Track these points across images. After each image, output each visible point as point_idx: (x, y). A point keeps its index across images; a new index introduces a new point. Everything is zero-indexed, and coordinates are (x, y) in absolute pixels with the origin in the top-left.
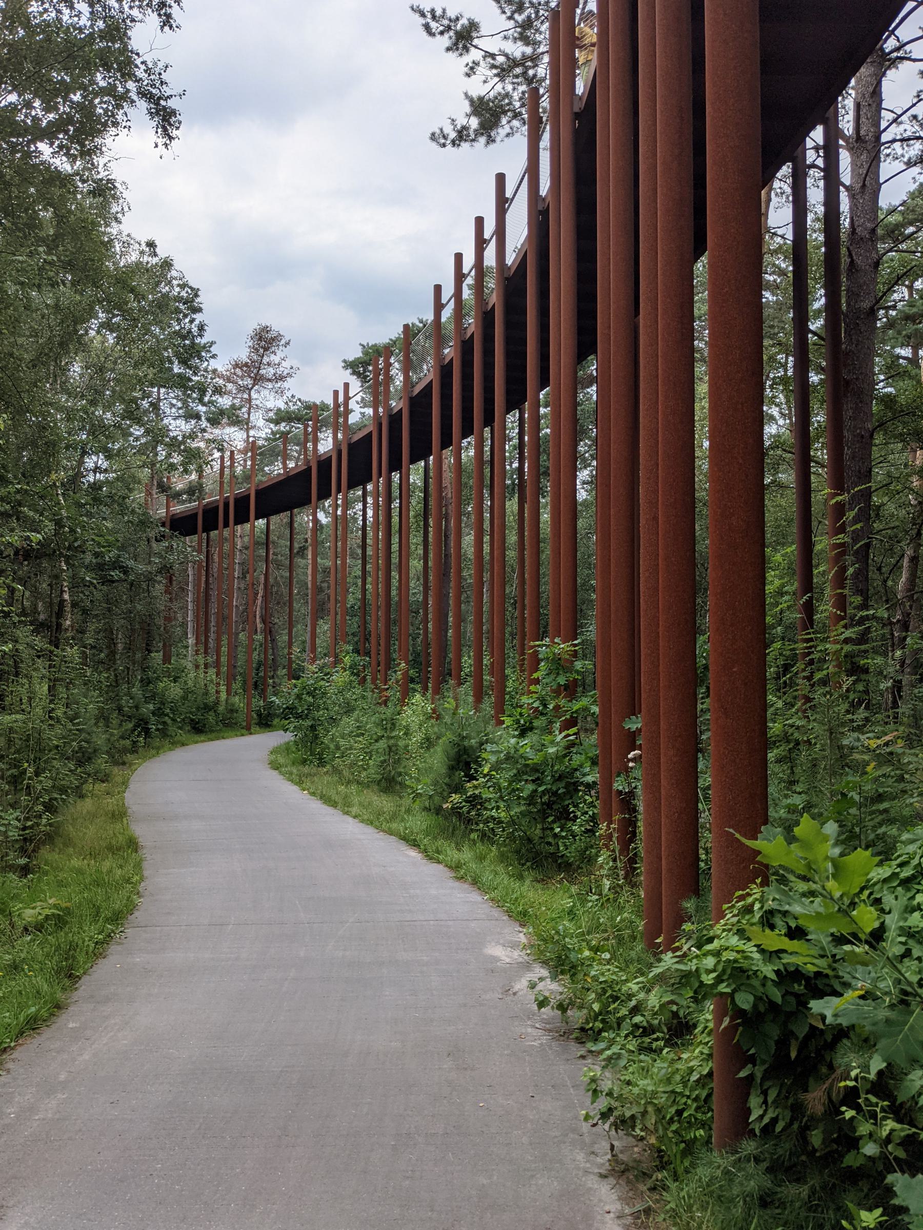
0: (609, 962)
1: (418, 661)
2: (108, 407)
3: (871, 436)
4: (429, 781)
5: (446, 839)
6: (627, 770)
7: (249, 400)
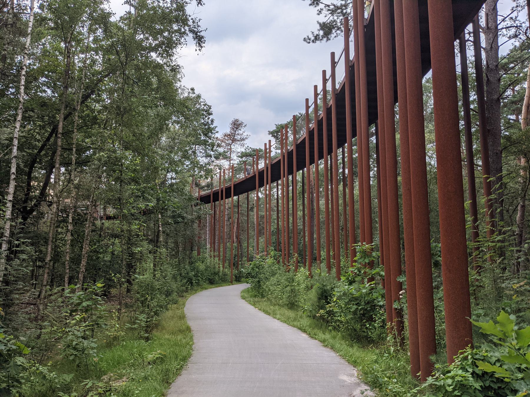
0: (396, 383)
1: (302, 255)
2: (176, 153)
3: (501, 153)
4: (310, 304)
5: (318, 329)
6: (399, 299)
7: (231, 149)
